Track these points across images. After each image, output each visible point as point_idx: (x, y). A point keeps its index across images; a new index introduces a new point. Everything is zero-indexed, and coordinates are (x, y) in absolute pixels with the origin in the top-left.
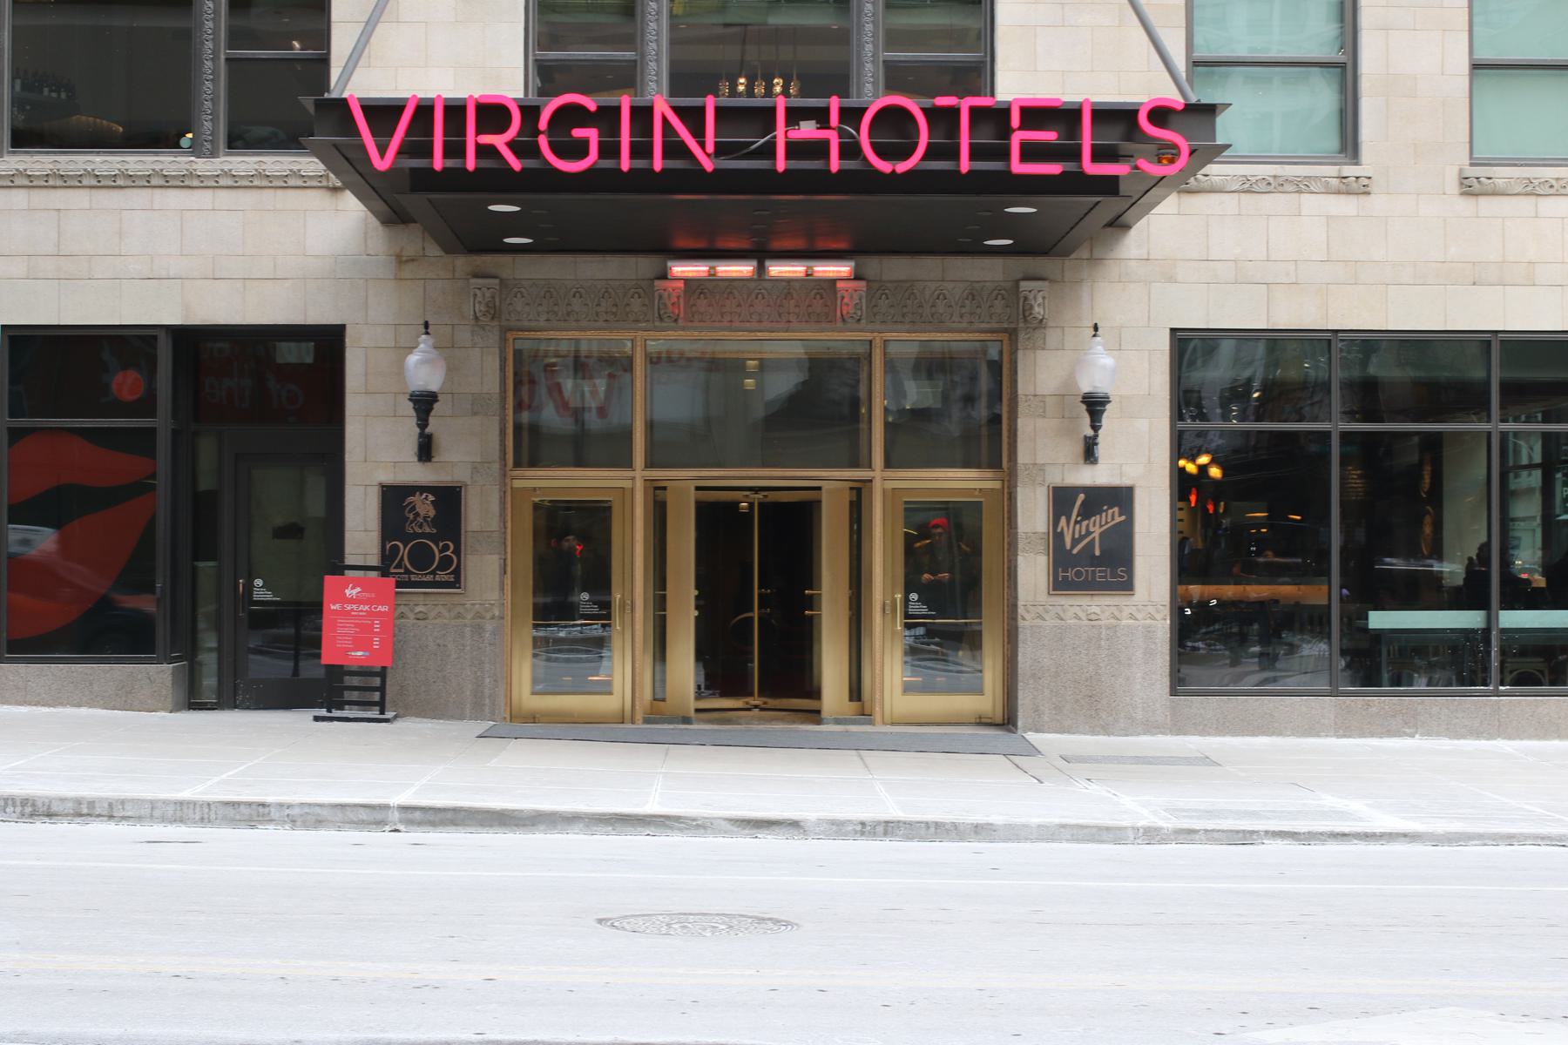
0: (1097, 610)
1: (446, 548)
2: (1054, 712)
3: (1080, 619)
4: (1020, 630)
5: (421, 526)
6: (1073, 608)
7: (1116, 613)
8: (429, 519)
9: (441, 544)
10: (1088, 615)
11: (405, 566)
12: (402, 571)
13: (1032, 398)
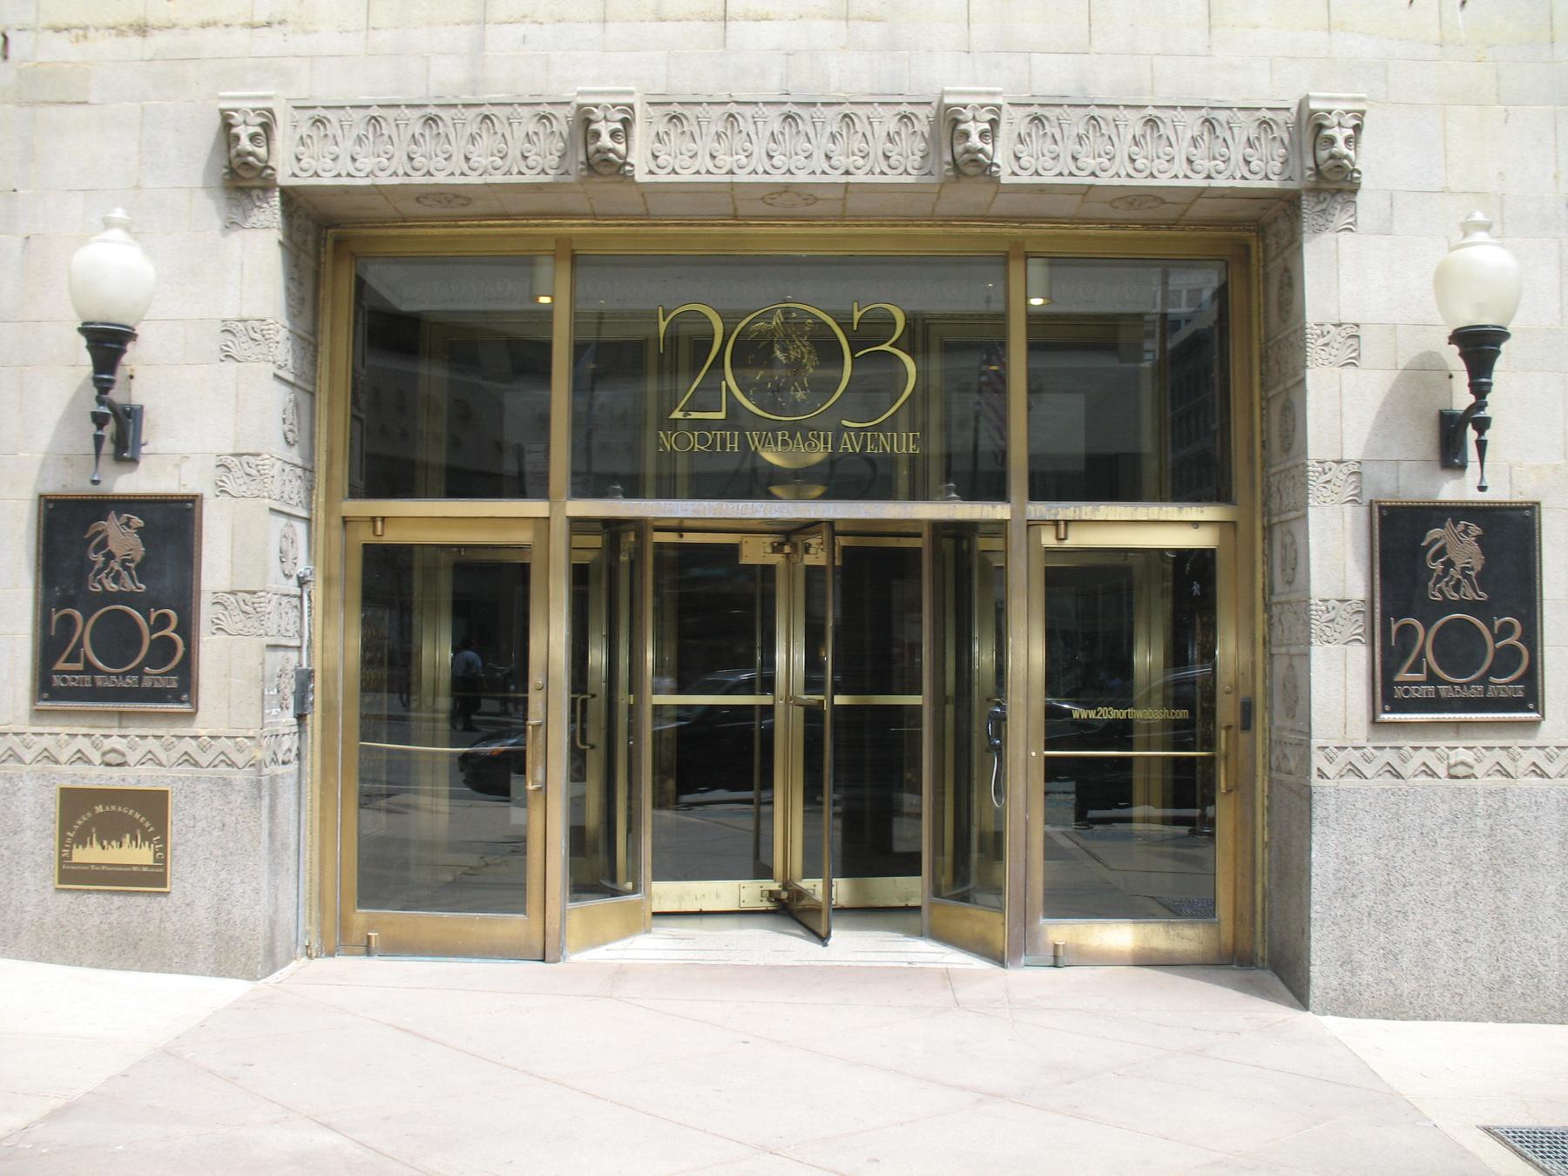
0: (1468, 757)
1: (163, 621)
2: (1382, 965)
3: (1434, 774)
4: (1315, 797)
5: (116, 578)
6: (1419, 753)
7: (1396, 763)
8: (132, 565)
9: (153, 616)
10: (1449, 767)
11: (1429, 668)
12: (1420, 677)
13: (1333, 329)
